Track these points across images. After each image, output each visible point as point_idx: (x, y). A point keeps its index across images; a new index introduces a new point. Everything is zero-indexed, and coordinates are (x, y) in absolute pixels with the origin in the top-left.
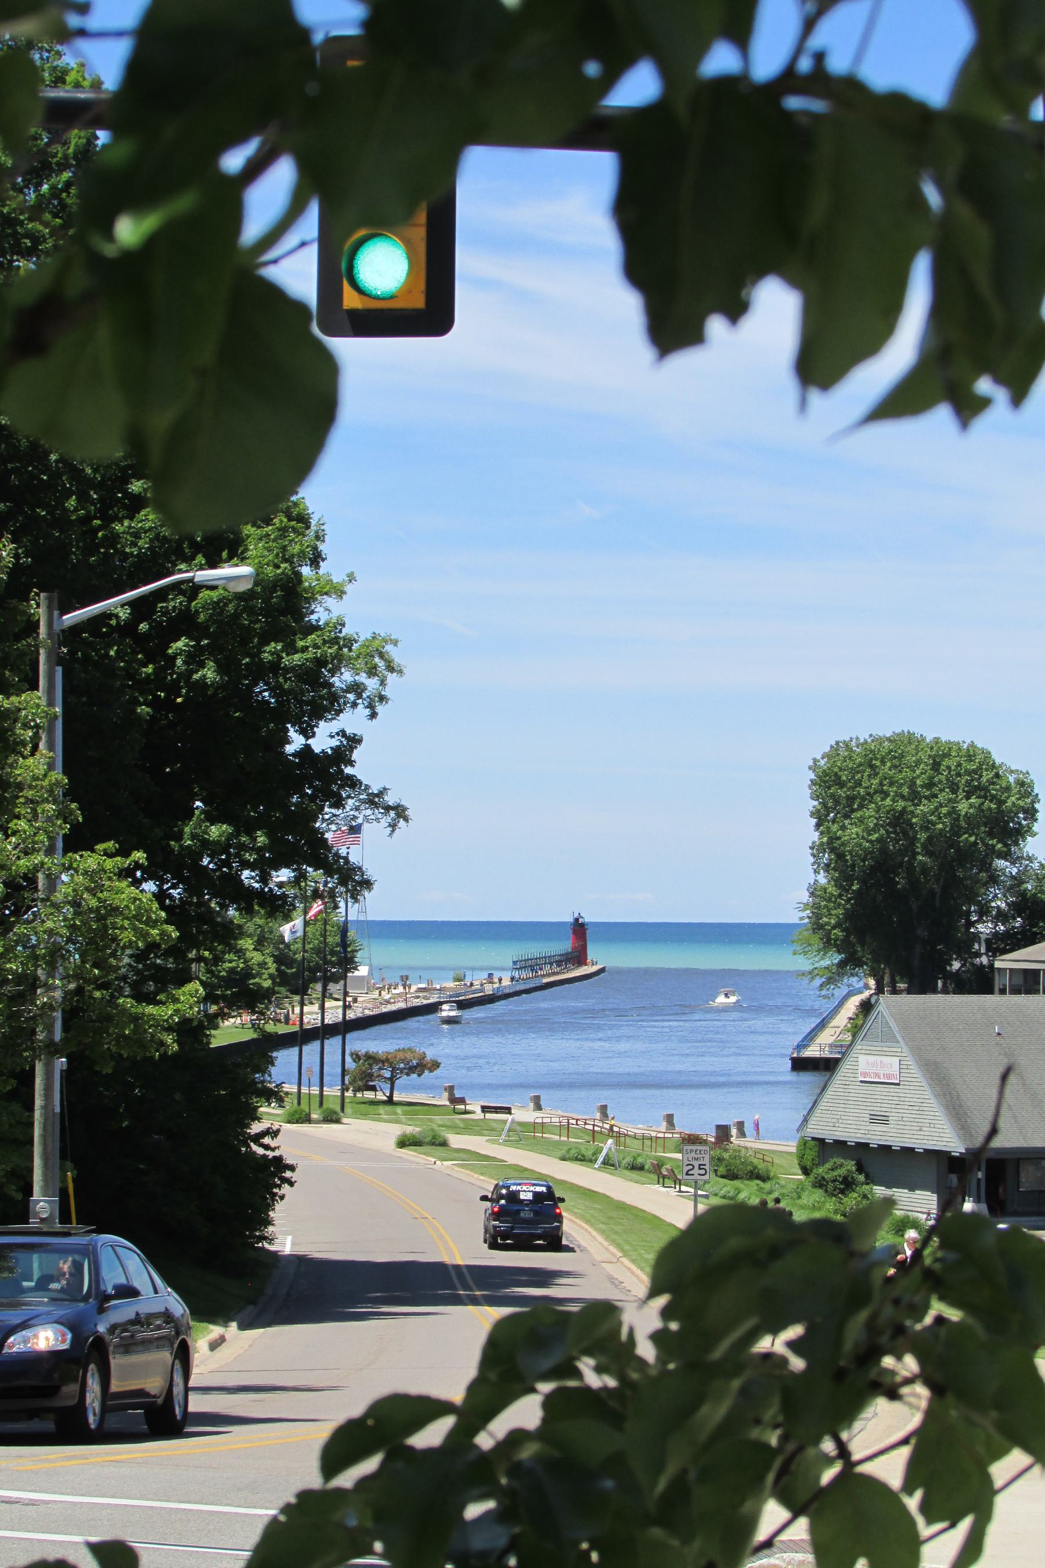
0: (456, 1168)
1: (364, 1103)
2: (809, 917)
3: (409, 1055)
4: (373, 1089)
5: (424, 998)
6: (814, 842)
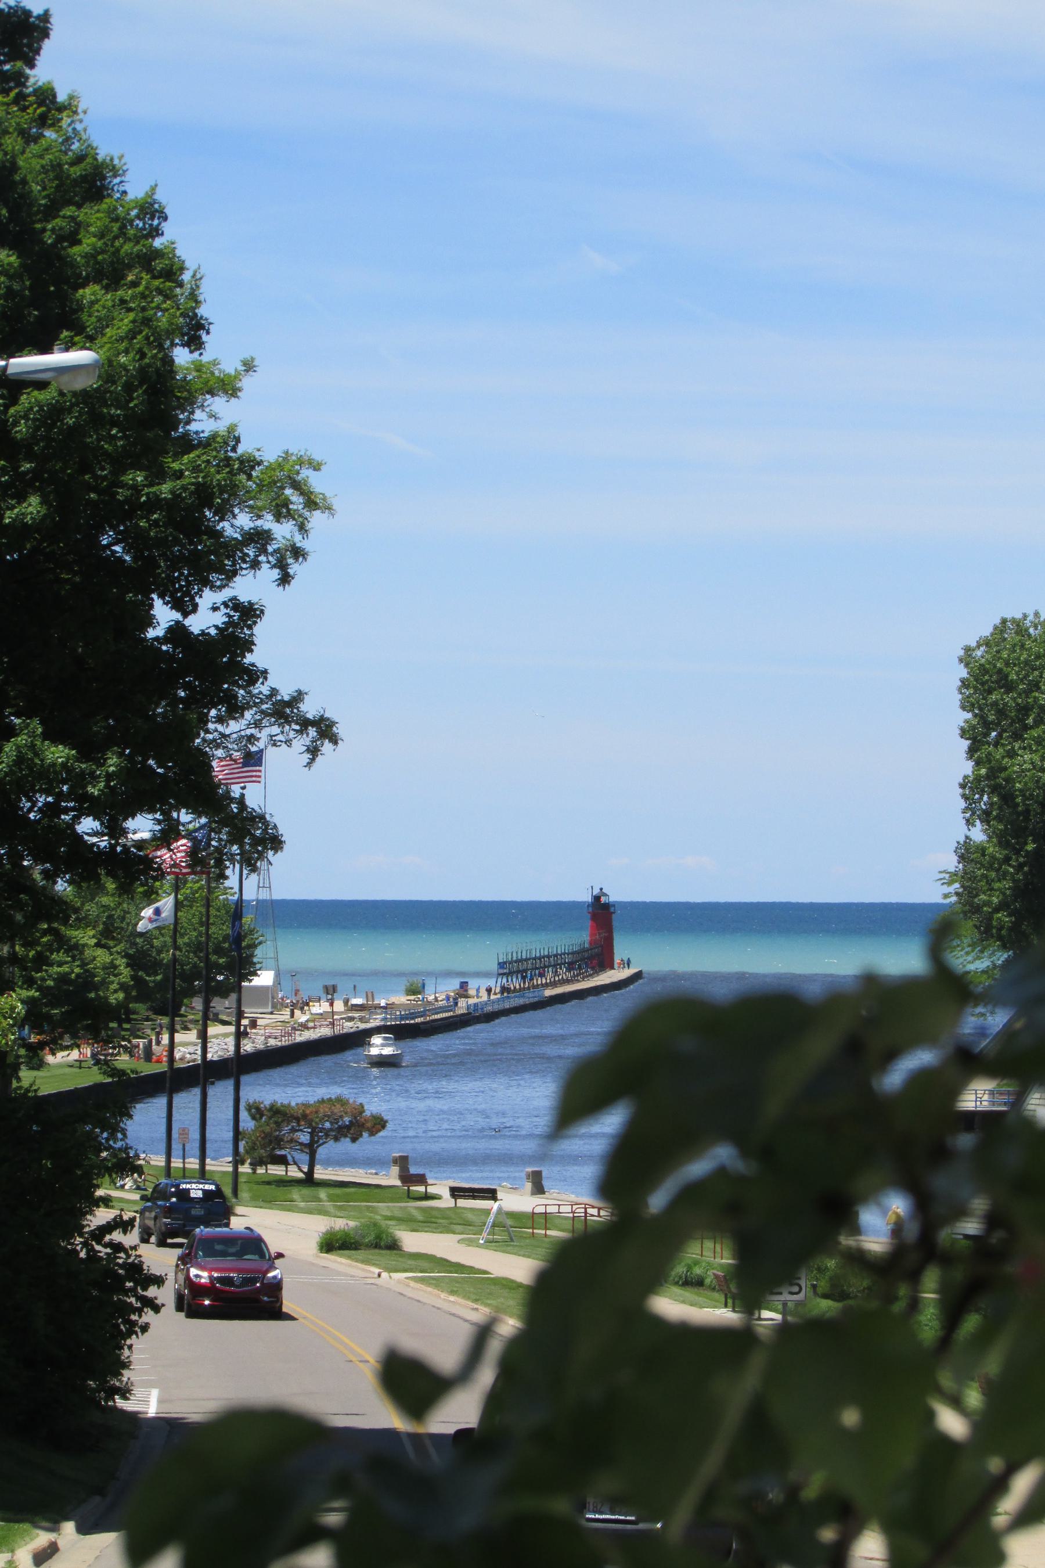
0: (412, 1284)
1: (269, 1183)
2: (957, 894)
3: (338, 1109)
4: (283, 1161)
5: (362, 1020)
6: (966, 777)
